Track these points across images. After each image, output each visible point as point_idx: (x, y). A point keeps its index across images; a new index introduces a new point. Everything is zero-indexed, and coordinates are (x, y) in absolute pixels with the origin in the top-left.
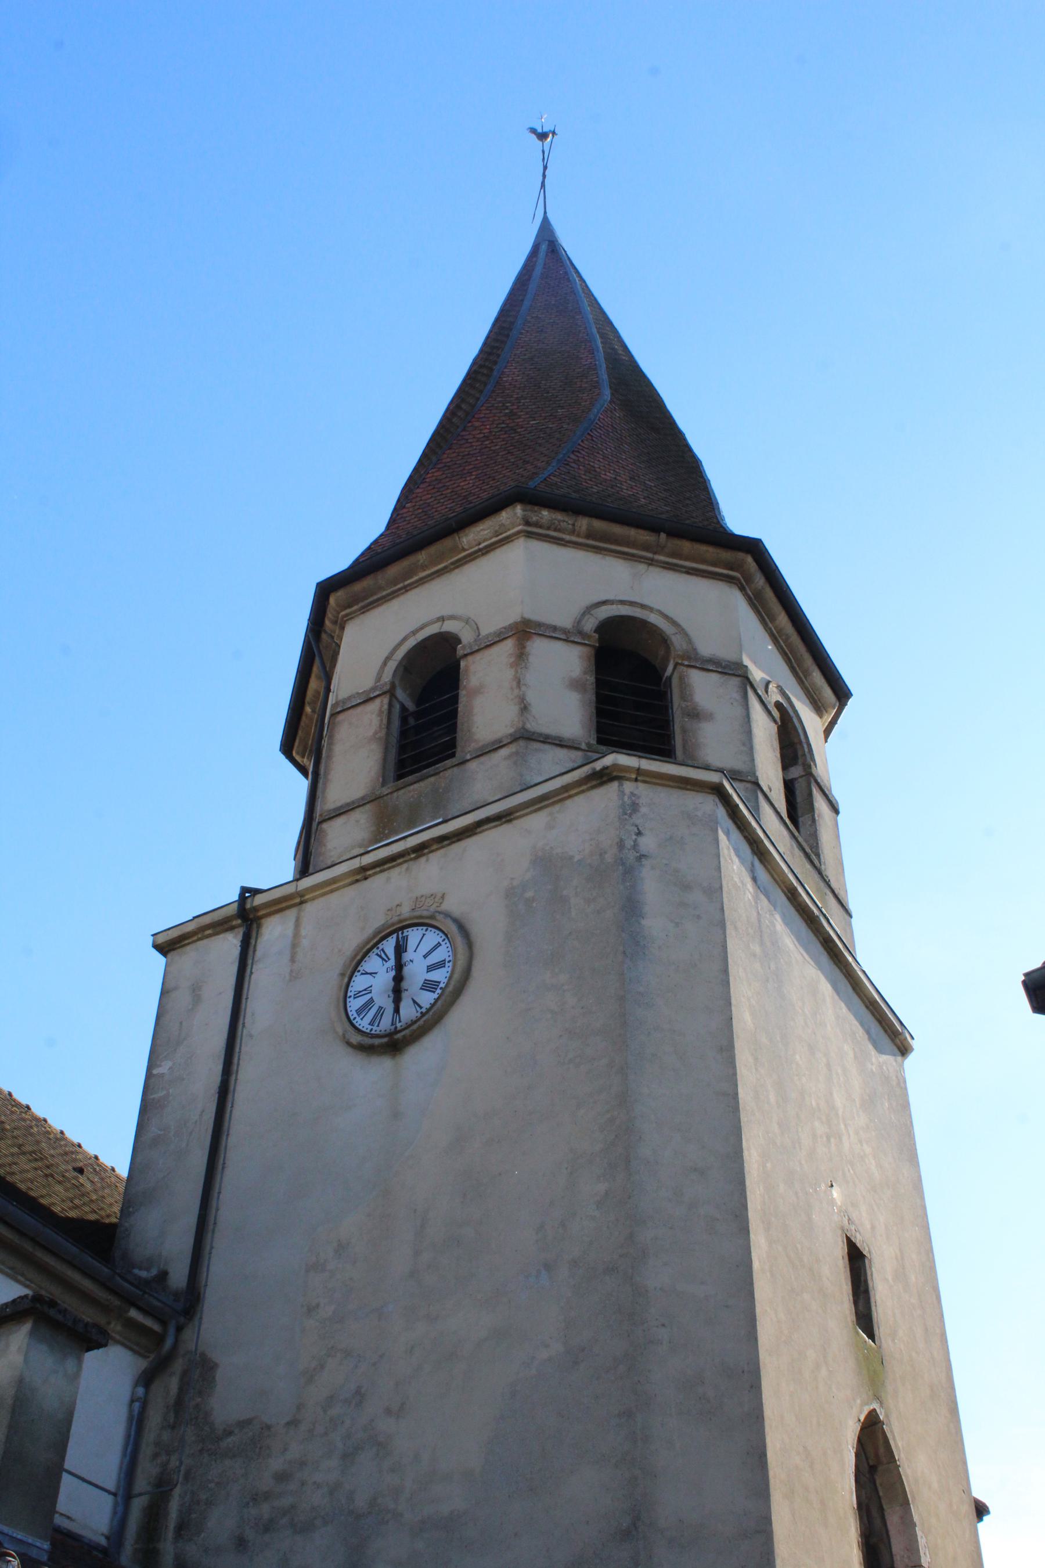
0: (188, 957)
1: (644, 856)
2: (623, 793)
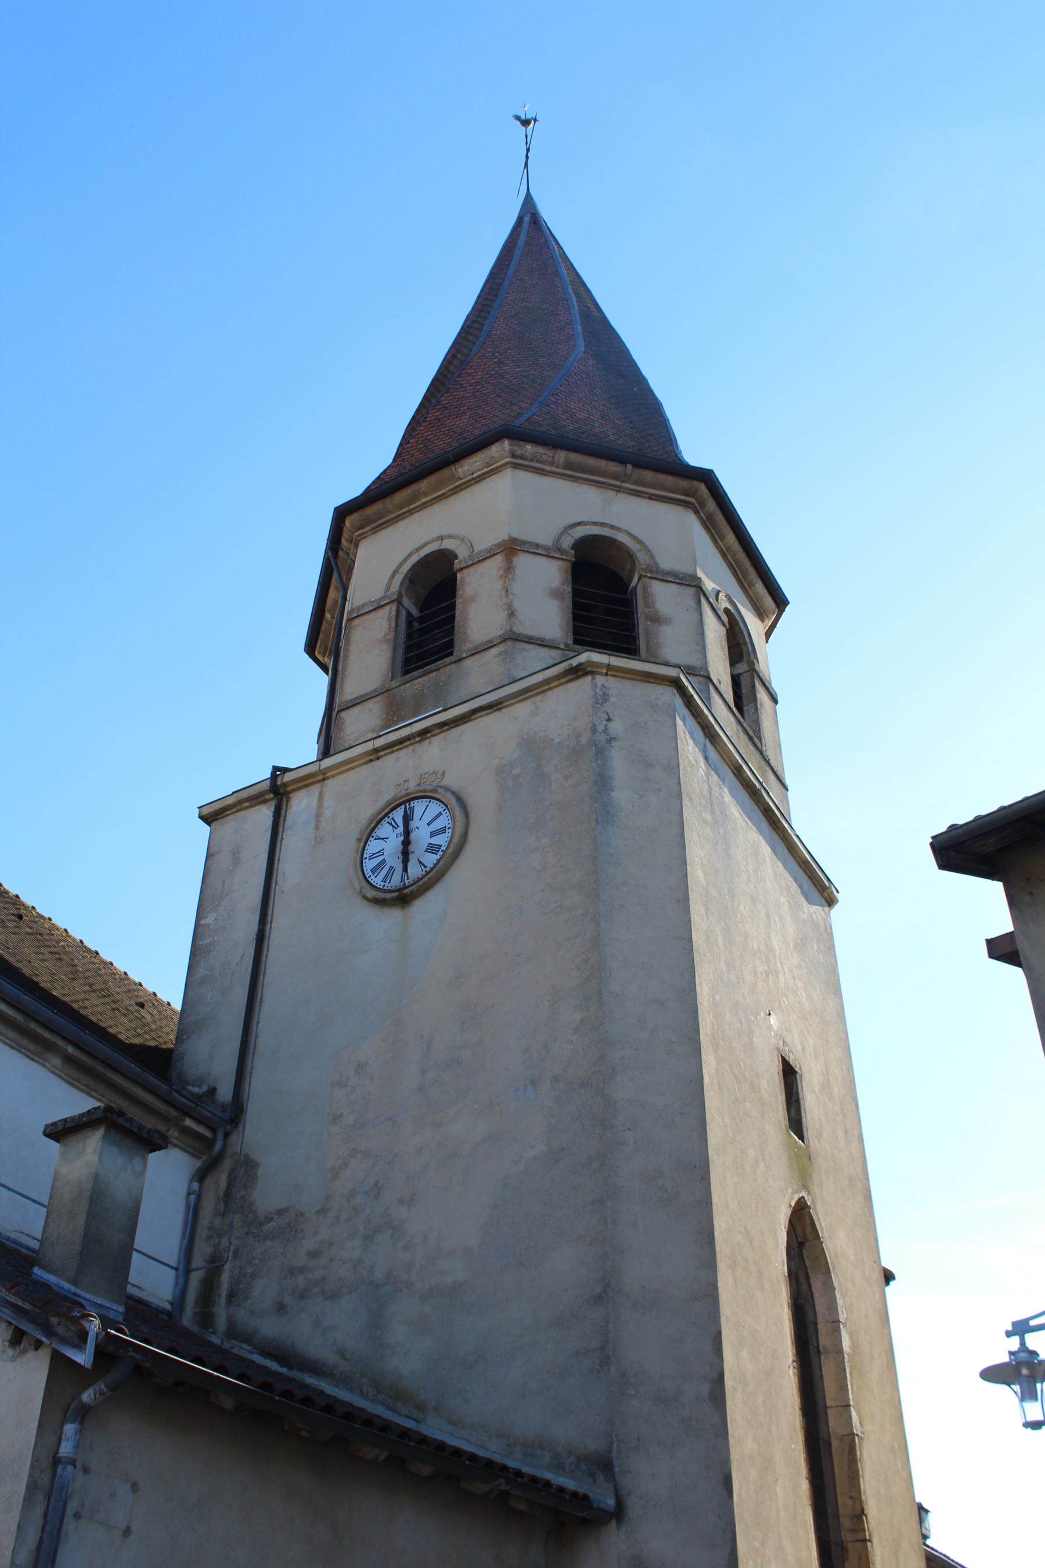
0: (229, 825)
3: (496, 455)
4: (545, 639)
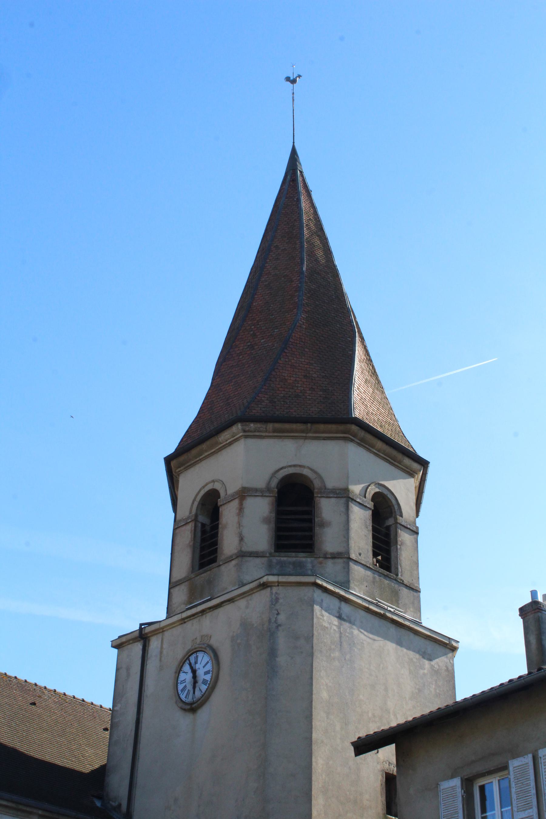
0: (126, 650)
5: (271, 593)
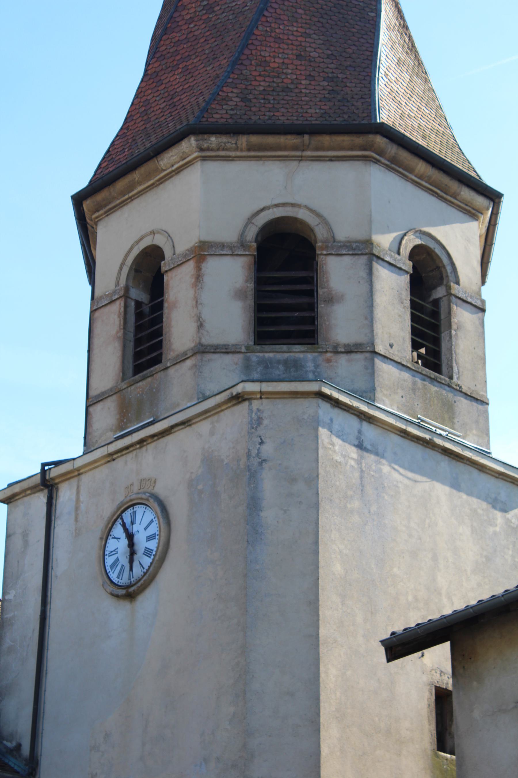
0: (21, 505)
1: (265, 460)
2: (251, 410)
3: (187, 150)
4: (228, 345)
5: (251, 410)
